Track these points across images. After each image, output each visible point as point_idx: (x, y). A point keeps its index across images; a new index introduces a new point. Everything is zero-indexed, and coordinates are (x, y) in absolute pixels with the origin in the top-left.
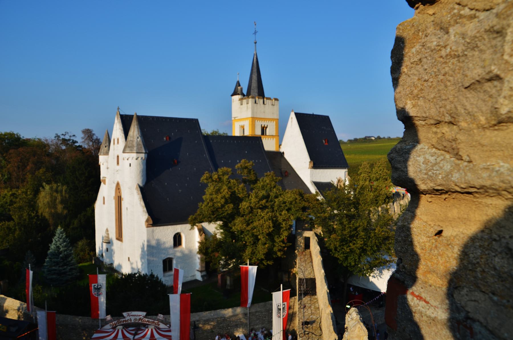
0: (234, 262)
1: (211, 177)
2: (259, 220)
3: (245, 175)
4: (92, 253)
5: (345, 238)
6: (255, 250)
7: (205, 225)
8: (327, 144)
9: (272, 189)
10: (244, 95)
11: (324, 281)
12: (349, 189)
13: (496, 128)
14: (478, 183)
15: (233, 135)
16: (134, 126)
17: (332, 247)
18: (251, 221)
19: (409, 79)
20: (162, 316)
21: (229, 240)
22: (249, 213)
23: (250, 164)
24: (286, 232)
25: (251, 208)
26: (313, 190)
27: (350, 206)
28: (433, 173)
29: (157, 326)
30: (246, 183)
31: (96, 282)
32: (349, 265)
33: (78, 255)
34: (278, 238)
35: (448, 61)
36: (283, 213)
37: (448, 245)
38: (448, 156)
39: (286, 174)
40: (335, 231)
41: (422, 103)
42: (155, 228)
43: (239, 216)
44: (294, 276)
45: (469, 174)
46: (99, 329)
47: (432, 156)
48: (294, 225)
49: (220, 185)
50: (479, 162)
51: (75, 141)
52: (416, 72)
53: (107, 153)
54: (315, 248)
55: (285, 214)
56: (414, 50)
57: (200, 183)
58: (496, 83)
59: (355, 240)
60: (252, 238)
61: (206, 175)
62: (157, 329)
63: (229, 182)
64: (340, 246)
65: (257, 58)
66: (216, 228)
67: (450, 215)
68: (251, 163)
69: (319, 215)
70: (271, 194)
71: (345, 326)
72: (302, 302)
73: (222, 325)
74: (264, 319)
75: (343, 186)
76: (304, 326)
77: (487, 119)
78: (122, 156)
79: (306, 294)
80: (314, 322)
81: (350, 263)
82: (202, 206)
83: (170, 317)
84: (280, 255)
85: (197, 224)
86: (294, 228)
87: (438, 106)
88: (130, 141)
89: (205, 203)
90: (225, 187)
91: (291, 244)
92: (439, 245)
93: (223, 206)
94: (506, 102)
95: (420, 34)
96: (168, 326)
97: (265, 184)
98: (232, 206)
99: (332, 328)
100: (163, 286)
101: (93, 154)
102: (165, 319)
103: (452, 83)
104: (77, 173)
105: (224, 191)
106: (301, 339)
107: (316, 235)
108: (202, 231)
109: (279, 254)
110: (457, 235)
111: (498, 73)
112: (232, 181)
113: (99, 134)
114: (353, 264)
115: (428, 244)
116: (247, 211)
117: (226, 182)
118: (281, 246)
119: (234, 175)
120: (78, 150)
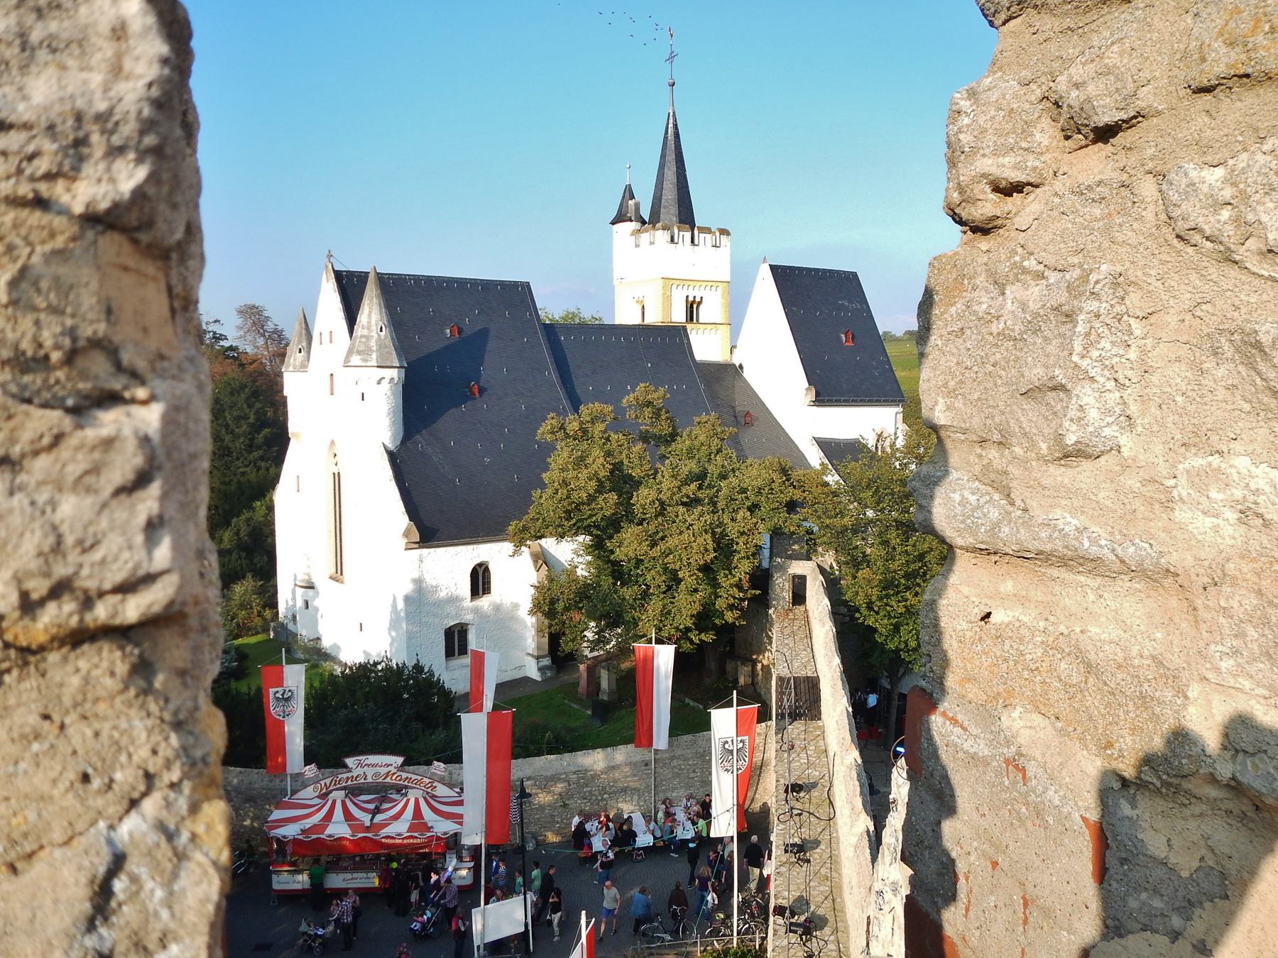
0: (620, 635)
1: (562, 428)
2: (681, 533)
3: (645, 422)
4: (268, 613)
5: (893, 578)
6: (670, 607)
7: (549, 544)
8: (850, 344)
9: (713, 456)
10: (644, 223)
11: (840, 683)
12: (904, 458)
13: (1063, 462)
14: (1035, 546)
15: (617, 322)
16: (371, 300)
17: (860, 601)
18: (661, 534)
19: (944, 359)
20: (442, 765)
21: (607, 582)
22: (656, 517)
23: (658, 395)
24: (746, 562)
25: (662, 503)
26: (815, 457)
27: (908, 499)
28: (973, 523)
29: (429, 790)
30: (649, 443)
31: (280, 682)
32: (902, 646)
33: (233, 619)
34: (726, 576)
35: (1000, 343)
36: (739, 517)
37: (997, 638)
38: (996, 496)
39: (748, 419)
40: (869, 562)
41: (961, 406)
42: (425, 551)
43: (631, 522)
44: (767, 671)
45: (1022, 531)
46: (286, 799)
47: (973, 494)
48: (768, 546)
49: (585, 445)
50: (1039, 515)
51: (221, 335)
52: (955, 351)
53: (303, 367)
54: (818, 603)
55: (744, 518)
56: (953, 310)
57: (537, 442)
58: (1062, 395)
59: (919, 585)
60: (664, 578)
61: (551, 422)
62: (431, 798)
63: (608, 439)
64: (881, 599)
65: (676, 126)
66: (575, 552)
67: (1002, 589)
68: (662, 390)
69: (828, 521)
70: (710, 468)
71: (891, 797)
72: (785, 736)
73: (589, 789)
74: (692, 775)
75: (888, 450)
76: (790, 795)
77: (1049, 448)
78: (343, 375)
79: (795, 716)
80: (814, 785)
81: (906, 642)
82: (541, 497)
83: (462, 768)
84: (730, 620)
85: (528, 542)
86: (766, 553)
87: (983, 415)
88: (362, 336)
89: (549, 491)
90: (597, 452)
91: (758, 592)
92: (984, 637)
93: (592, 499)
94: (1074, 428)
95: (966, 282)
96: (458, 790)
97: (696, 443)
98: (616, 497)
99: (858, 802)
100: (445, 694)
101: (268, 368)
102: (450, 774)
103: (1004, 381)
104: (227, 414)
105: (594, 460)
106: (782, 826)
107: (822, 570)
108: (541, 559)
109: (729, 617)
110: (1010, 623)
111: (1063, 382)
112: (614, 436)
113: (281, 317)
114: (913, 644)
115: (969, 634)
116: (651, 511)
117: (601, 438)
118: (735, 598)
119: (618, 423)
120: (228, 357)
